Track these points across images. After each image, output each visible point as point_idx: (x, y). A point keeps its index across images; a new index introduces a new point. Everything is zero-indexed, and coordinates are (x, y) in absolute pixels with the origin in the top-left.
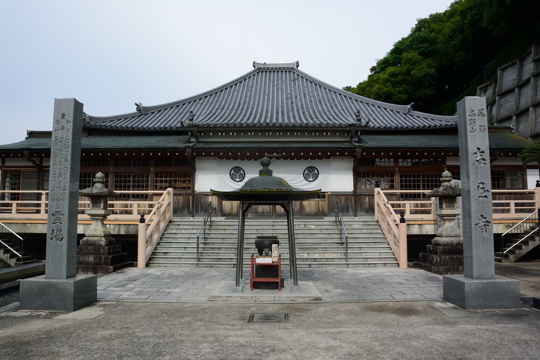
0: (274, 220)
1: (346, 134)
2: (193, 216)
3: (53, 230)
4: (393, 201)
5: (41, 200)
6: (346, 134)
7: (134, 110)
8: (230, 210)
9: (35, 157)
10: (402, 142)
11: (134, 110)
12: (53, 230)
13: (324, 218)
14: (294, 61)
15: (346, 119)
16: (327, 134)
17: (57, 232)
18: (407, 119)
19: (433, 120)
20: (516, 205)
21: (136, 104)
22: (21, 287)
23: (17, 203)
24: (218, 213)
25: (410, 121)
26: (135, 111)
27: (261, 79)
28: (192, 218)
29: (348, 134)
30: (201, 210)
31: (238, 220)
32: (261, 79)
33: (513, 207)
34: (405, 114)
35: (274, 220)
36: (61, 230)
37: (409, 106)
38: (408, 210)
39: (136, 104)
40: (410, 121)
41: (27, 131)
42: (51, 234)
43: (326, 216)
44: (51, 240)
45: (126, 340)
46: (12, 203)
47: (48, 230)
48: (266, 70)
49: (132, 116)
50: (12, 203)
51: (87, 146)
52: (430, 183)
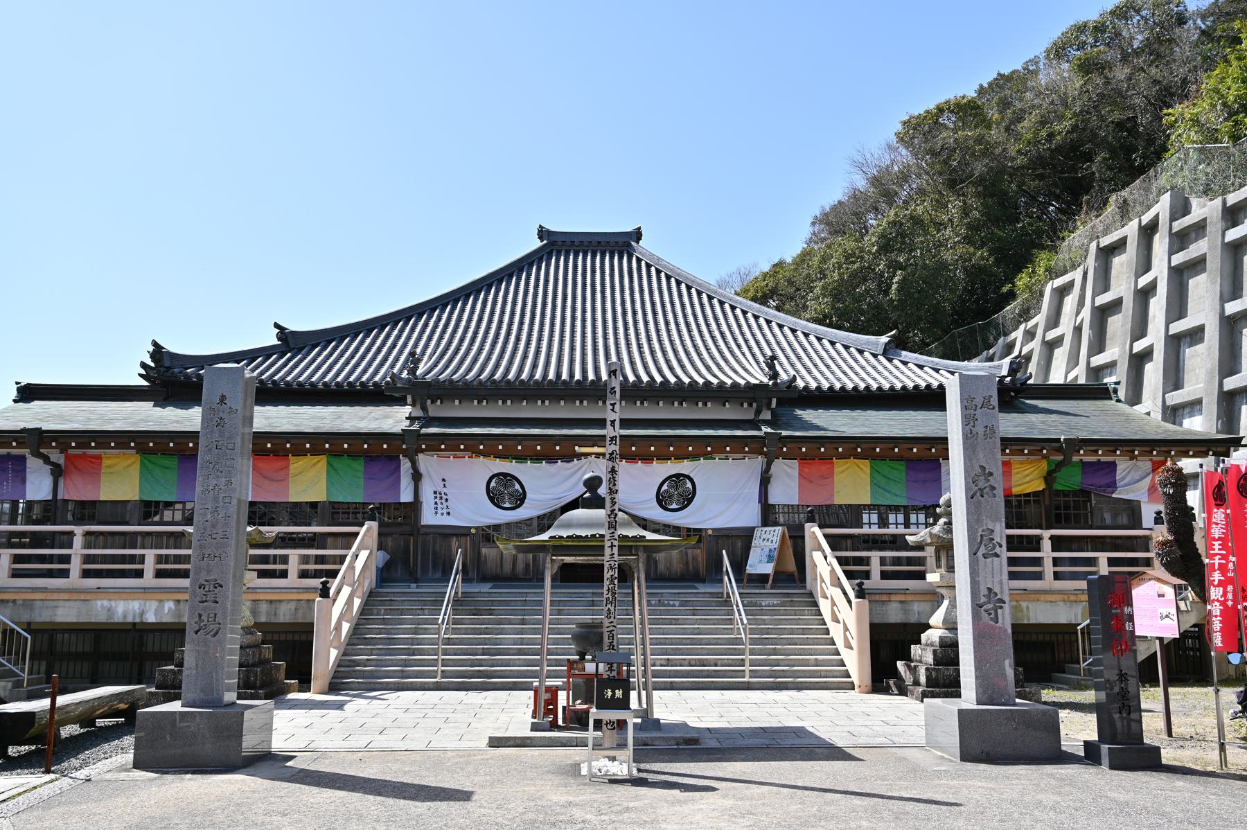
0: (595, 591)
1: (745, 405)
2: (416, 581)
3: (200, 616)
4: (847, 550)
5: (70, 547)
6: (745, 405)
7: (272, 340)
8: (496, 567)
9: (54, 448)
10: (867, 422)
11: (272, 340)
12: (200, 616)
13: (696, 585)
14: (629, 228)
15: (746, 370)
16: (706, 405)
17: (208, 618)
18: (880, 368)
19: (937, 371)
20: (160, 559)
21: (277, 326)
22: (1188, 692)
23: (881, 557)
24: (470, 573)
25: (886, 374)
26: (275, 341)
27: (575, 267)
28: (415, 585)
29: (750, 405)
30: (435, 567)
31: (630, 591)
32: (575, 267)
33: (149, 566)
34: (875, 356)
35: (595, 591)
36: (215, 615)
37: (884, 339)
38: (875, 568)
39: (277, 326)
40: (886, 374)
41: (17, 383)
42: (196, 623)
43: (702, 581)
44: (194, 634)
45: (1124, 782)
46: (144, 556)
47: (191, 615)
48: (568, 248)
49: (266, 352)
50: (144, 556)
51: (175, 425)
52: (1063, 512)
